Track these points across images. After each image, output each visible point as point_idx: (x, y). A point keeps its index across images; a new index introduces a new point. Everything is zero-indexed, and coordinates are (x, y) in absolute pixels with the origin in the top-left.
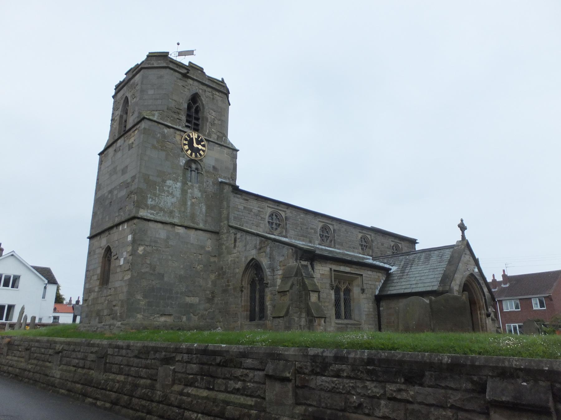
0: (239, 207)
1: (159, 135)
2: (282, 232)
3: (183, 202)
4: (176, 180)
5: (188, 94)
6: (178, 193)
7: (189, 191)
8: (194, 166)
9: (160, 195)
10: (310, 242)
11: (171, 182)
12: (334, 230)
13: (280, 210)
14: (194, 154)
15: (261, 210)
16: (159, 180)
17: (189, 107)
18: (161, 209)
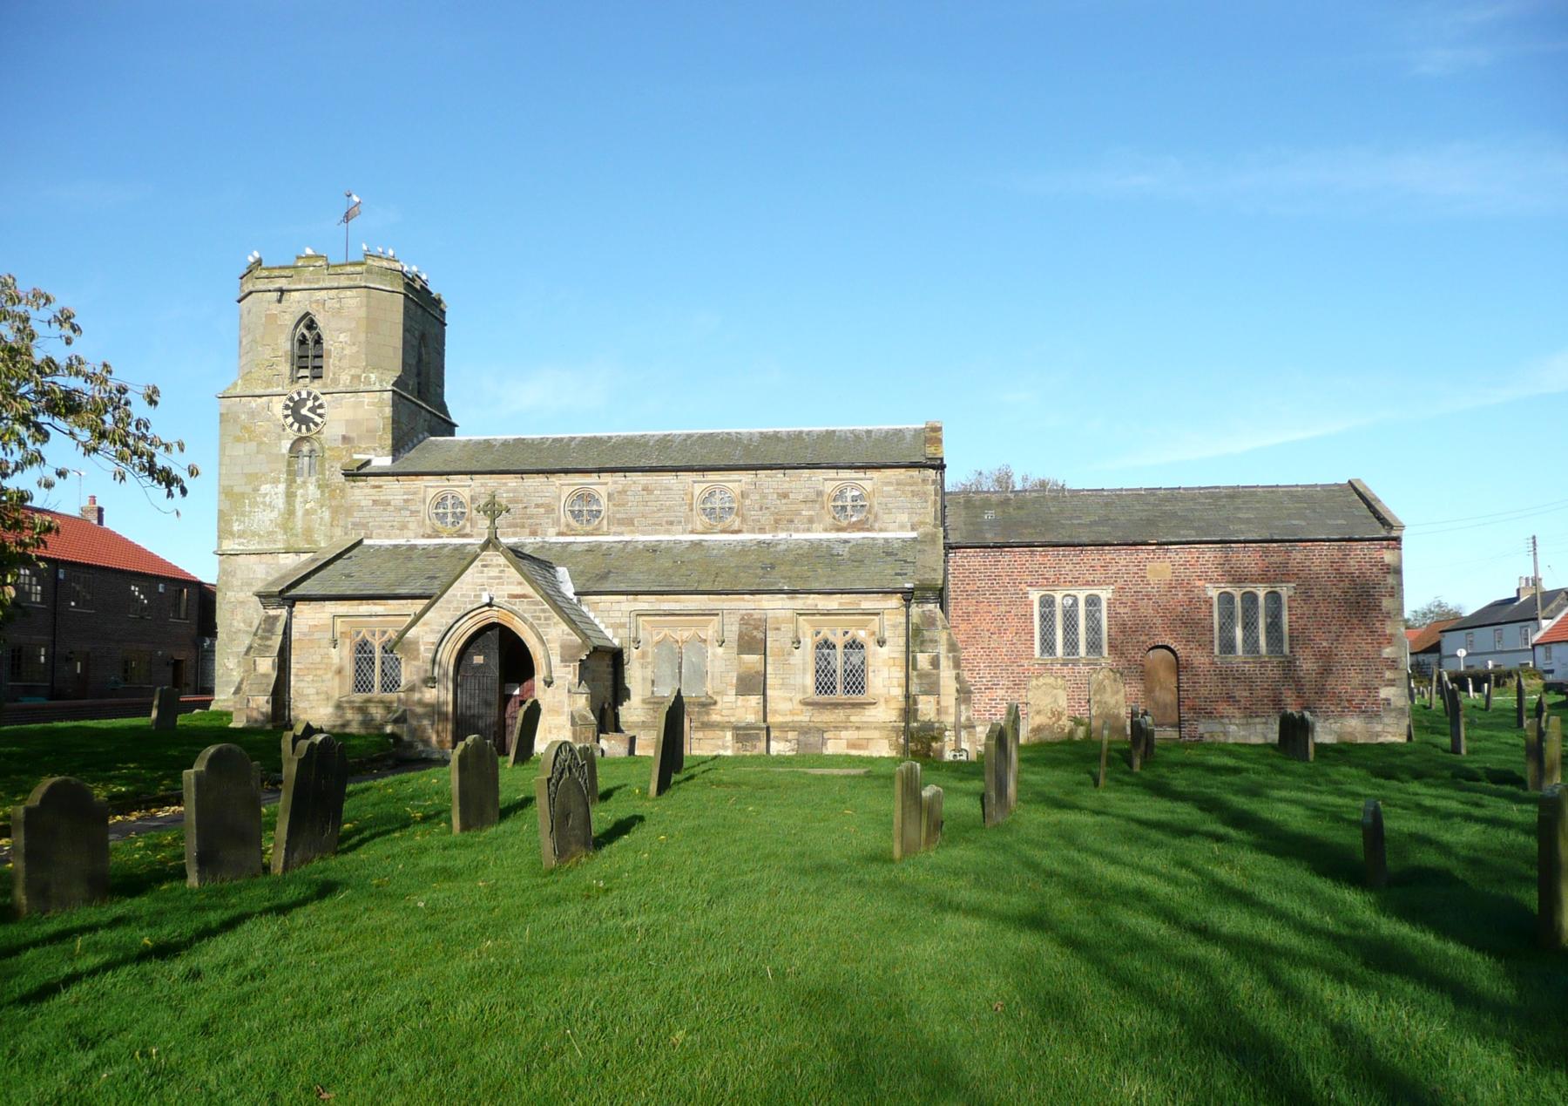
0: (363, 503)
1: (243, 417)
2: (464, 527)
4: (276, 481)
6: (280, 502)
7: (300, 492)
8: (306, 448)
9: (250, 512)
10: (534, 533)
11: (268, 486)
12: (610, 496)
13: (458, 486)
14: (304, 427)
15: (410, 497)
16: (248, 489)
18: (254, 534)
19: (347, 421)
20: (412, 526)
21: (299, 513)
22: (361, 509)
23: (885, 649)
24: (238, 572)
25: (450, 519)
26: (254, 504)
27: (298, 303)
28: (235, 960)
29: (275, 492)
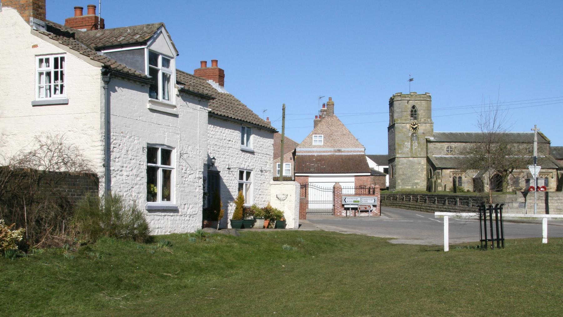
3: (412, 149)
4: (408, 142)
5: (410, 106)
6: (409, 146)
7: (414, 144)
8: (415, 135)
17: (412, 111)
18: (404, 153)
19: (424, 129)
20: (442, 153)
21: (414, 149)
22: (431, 149)
23: (553, 179)
24: (400, 161)
25: (449, 151)
26: (403, 147)
27: (412, 103)
28: (136, 184)
29: (408, 144)
